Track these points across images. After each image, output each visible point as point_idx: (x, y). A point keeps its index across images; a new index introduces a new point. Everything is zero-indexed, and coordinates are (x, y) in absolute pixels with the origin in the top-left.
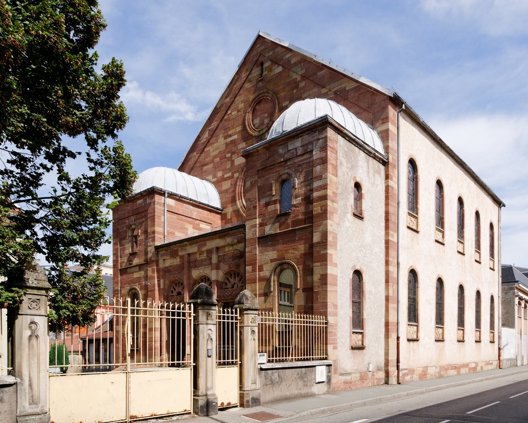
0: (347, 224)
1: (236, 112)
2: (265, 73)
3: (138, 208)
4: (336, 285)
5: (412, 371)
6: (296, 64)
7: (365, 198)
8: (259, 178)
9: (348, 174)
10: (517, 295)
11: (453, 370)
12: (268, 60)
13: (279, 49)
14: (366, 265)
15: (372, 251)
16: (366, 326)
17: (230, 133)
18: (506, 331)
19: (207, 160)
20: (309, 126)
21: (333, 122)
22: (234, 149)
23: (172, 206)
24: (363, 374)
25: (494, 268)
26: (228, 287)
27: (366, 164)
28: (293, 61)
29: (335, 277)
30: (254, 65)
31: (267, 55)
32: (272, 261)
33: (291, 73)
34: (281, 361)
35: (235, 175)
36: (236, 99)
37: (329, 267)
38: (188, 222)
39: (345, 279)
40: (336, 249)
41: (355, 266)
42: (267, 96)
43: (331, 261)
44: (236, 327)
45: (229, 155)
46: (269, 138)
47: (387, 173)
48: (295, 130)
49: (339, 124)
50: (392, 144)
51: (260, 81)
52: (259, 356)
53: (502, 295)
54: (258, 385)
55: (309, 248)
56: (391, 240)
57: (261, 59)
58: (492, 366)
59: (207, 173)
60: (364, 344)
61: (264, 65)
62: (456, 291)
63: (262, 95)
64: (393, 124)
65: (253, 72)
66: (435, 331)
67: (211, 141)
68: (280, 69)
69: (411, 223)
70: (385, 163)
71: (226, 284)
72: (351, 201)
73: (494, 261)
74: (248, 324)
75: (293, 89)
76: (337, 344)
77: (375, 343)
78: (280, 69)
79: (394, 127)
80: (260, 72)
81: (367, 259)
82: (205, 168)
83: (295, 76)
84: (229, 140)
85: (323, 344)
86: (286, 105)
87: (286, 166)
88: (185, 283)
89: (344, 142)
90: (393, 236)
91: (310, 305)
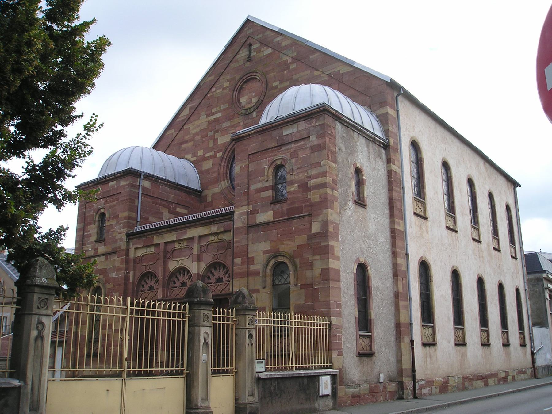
0: (349, 212)
1: (221, 90)
2: (254, 54)
3: (109, 191)
4: (339, 281)
5: (430, 383)
6: (286, 47)
7: (367, 184)
8: (249, 162)
9: (347, 160)
10: (547, 287)
11: (480, 381)
12: (257, 42)
13: (269, 32)
14: (371, 257)
15: (377, 241)
16: (375, 327)
17: (214, 110)
18: (537, 331)
19: (187, 138)
20: (305, 113)
21: (331, 110)
22: (217, 127)
23: (148, 188)
24: (373, 386)
25: (516, 256)
26: (211, 281)
27: (366, 149)
28: (283, 44)
29: (338, 272)
30: (242, 46)
31: (256, 37)
32: (264, 252)
33: (281, 55)
34: (280, 370)
35: (218, 154)
36: (221, 78)
37: (331, 261)
38: (164, 206)
39: (348, 273)
40: (337, 240)
41: (358, 258)
42: (256, 76)
43: (333, 254)
44: (232, 329)
45: (211, 133)
46: (263, 121)
47: (389, 158)
48: (290, 116)
49: (337, 111)
50: (392, 128)
51: (248, 61)
52: (256, 362)
53: (529, 288)
54: (256, 398)
55: (308, 239)
56: (397, 229)
57: (250, 41)
58: (526, 375)
59: (186, 151)
60: (373, 349)
61: (252, 46)
62: (475, 285)
63: (250, 75)
64: (392, 107)
65: (240, 52)
66: (455, 333)
67: (191, 119)
68: (270, 51)
69: (418, 209)
70: (386, 147)
71: (209, 278)
72: (353, 188)
73: (515, 249)
74: (246, 326)
75: (283, 70)
76: (342, 349)
77: (386, 349)
78: (270, 51)
79: (393, 111)
80: (247, 53)
81: (372, 250)
82: (184, 146)
83: (285, 58)
84: (212, 118)
85: (326, 350)
86: (276, 85)
87: (280, 151)
88: (160, 276)
89: (342, 128)
90: (399, 224)
91: (310, 303)
